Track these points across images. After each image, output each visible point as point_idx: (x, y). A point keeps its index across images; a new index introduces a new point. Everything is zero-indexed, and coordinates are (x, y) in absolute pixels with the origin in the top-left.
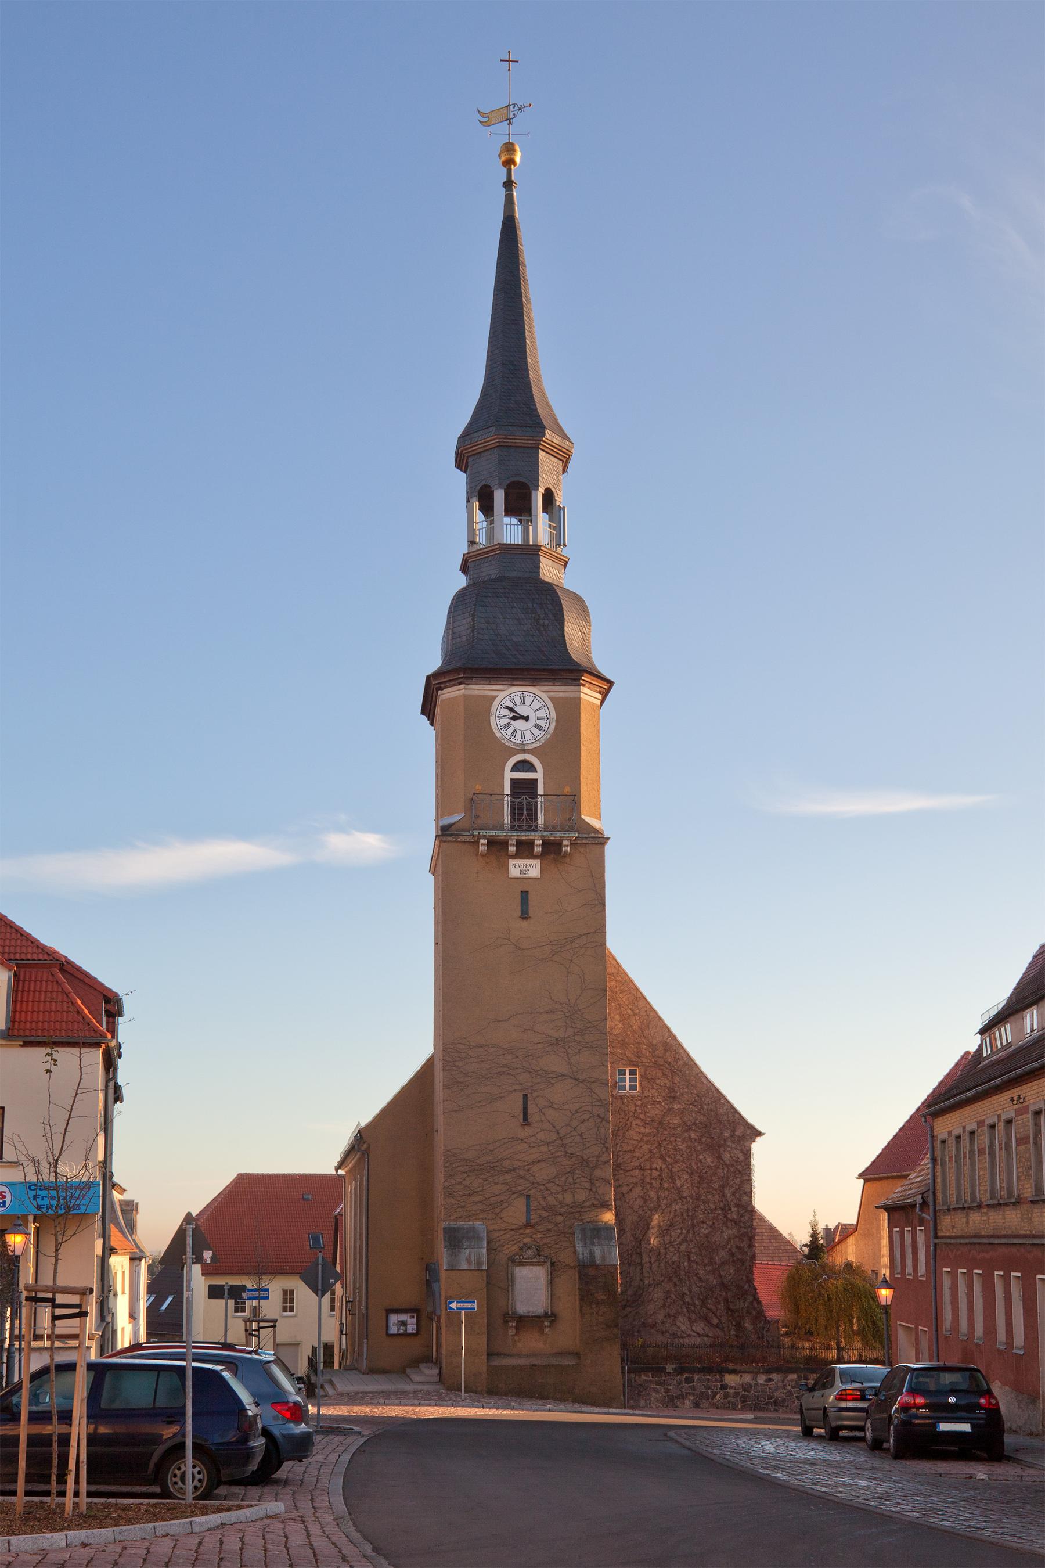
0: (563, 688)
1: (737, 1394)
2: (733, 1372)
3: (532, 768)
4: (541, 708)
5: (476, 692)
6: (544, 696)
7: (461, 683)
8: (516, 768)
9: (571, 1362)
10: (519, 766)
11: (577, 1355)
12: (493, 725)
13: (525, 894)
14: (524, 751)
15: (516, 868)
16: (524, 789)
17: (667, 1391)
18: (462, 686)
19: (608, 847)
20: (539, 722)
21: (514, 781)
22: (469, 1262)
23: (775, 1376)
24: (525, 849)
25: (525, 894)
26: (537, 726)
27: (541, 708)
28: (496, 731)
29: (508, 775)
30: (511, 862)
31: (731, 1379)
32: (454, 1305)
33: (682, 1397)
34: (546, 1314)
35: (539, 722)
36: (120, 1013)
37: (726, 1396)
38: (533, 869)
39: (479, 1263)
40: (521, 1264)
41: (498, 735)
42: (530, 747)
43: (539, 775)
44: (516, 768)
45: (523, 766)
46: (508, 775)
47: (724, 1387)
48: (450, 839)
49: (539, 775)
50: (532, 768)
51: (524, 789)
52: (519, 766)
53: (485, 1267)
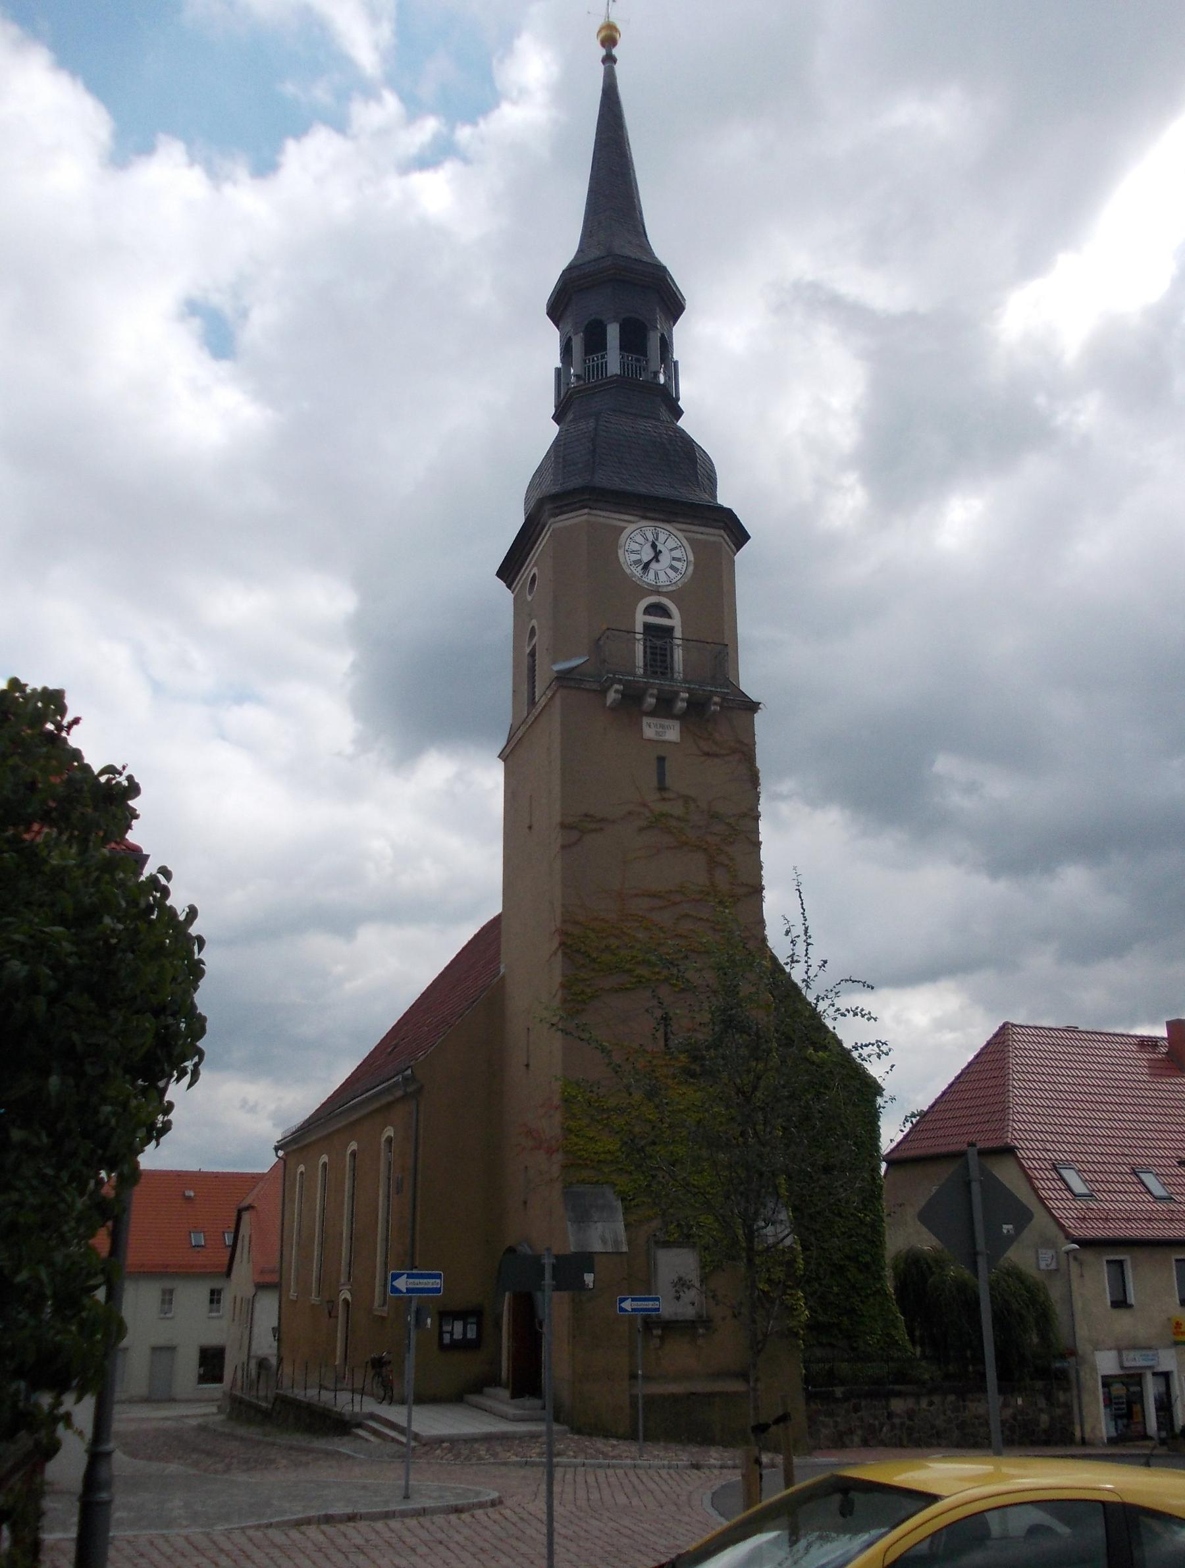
0: (702, 529)
1: (902, 1424)
2: (899, 1394)
3: (666, 613)
4: (676, 548)
5: (602, 520)
6: (680, 534)
7: (584, 507)
8: (649, 610)
9: (737, 1386)
10: (652, 609)
11: (744, 1376)
12: (622, 560)
13: (661, 760)
14: (659, 593)
15: (651, 729)
16: (658, 636)
17: (836, 1424)
18: (586, 511)
19: (758, 717)
20: (675, 563)
21: (647, 627)
22: (604, 1242)
23: (936, 1399)
24: (664, 707)
25: (661, 760)
26: (672, 567)
27: (676, 548)
28: (624, 567)
29: (640, 619)
30: (646, 720)
31: (897, 1405)
32: (627, 1305)
33: (851, 1432)
34: (701, 1317)
35: (675, 563)
36: (674, 306)
37: (893, 1427)
38: (672, 732)
39: (616, 1242)
40: (667, 1245)
41: (628, 571)
42: (665, 590)
43: (676, 621)
44: (649, 610)
45: (656, 609)
46: (640, 619)
47: (890, 1415)
48: (572, 684)
49: (676, 621)
50: (666, 613)
51: (658, 636)
52: (652, 609)
53: (625, 1249)
